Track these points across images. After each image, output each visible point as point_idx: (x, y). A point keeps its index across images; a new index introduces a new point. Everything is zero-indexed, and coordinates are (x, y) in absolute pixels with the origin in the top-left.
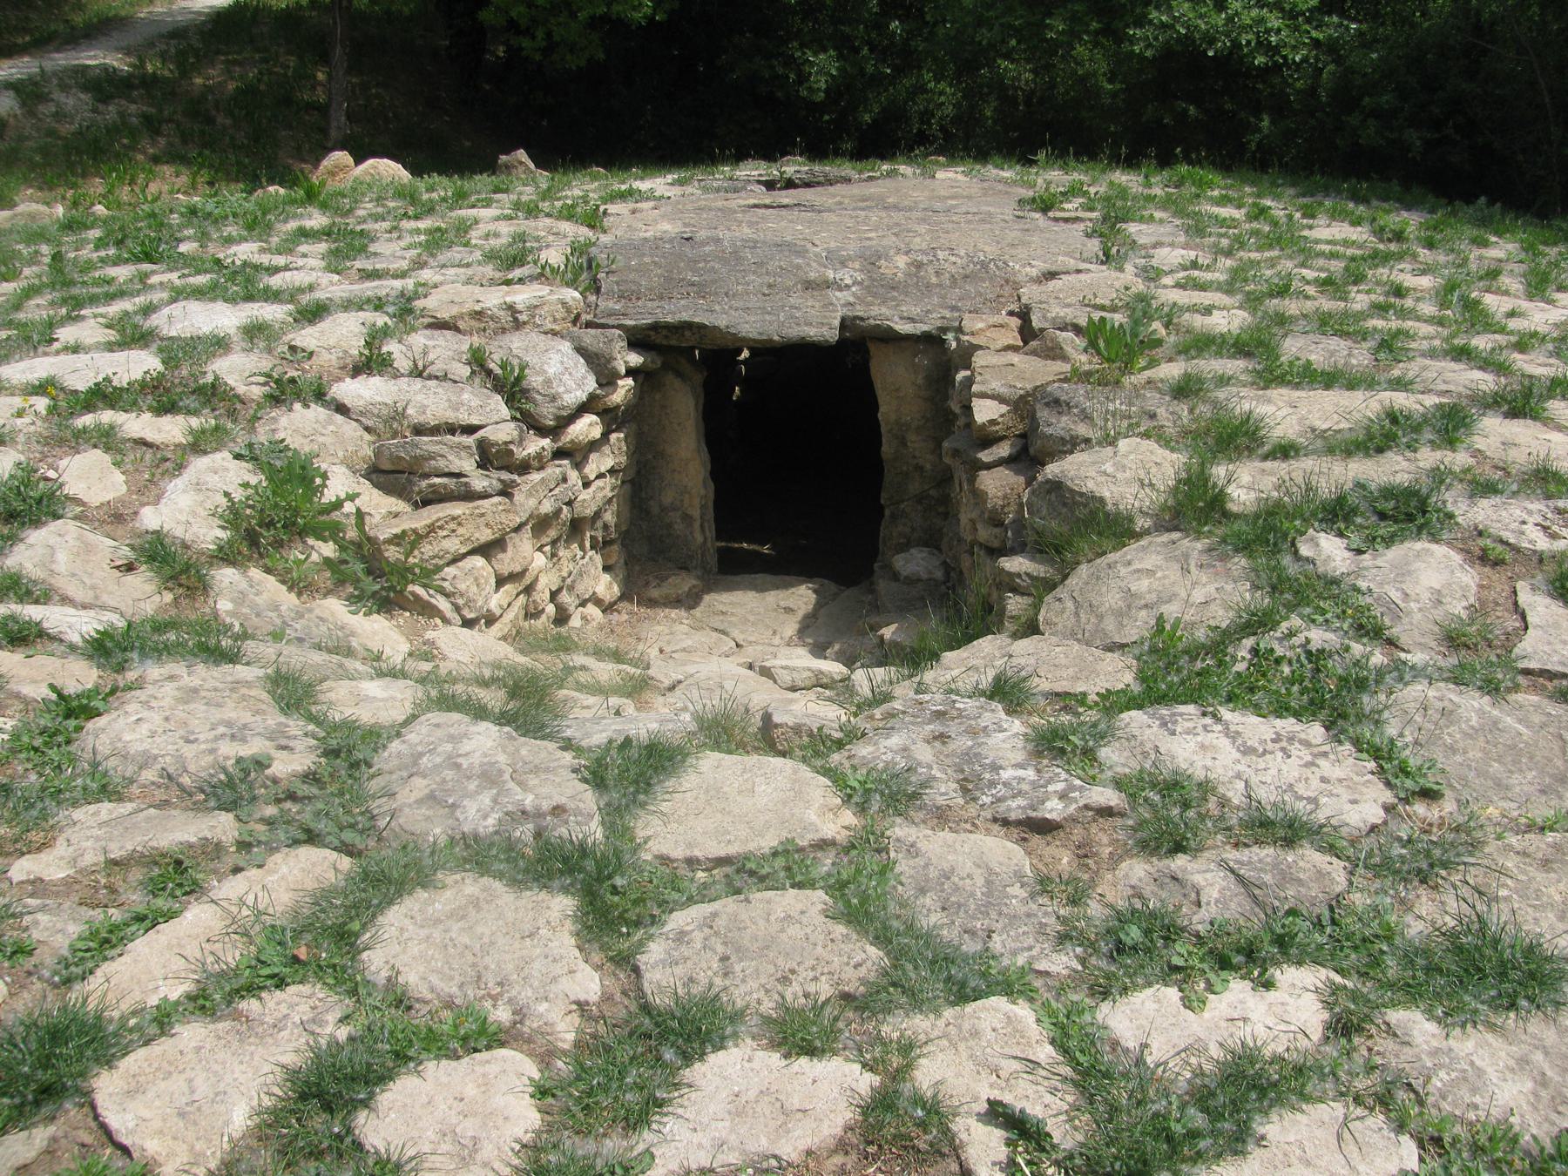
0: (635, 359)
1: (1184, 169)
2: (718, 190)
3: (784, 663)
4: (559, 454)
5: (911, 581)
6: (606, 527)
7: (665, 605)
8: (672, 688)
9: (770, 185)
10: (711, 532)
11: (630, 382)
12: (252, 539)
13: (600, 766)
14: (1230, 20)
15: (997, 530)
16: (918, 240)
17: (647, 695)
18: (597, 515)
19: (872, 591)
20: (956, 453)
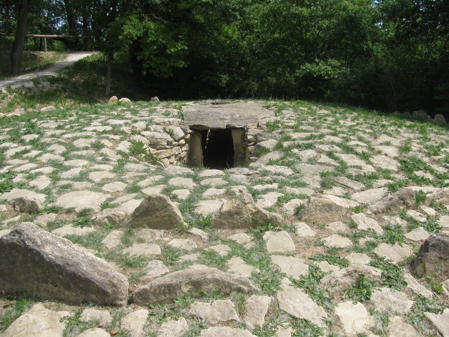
1: (299, 101)
4: (178, 145)
9: (213, 104)
12: (133, 152)
14: (319, 68)
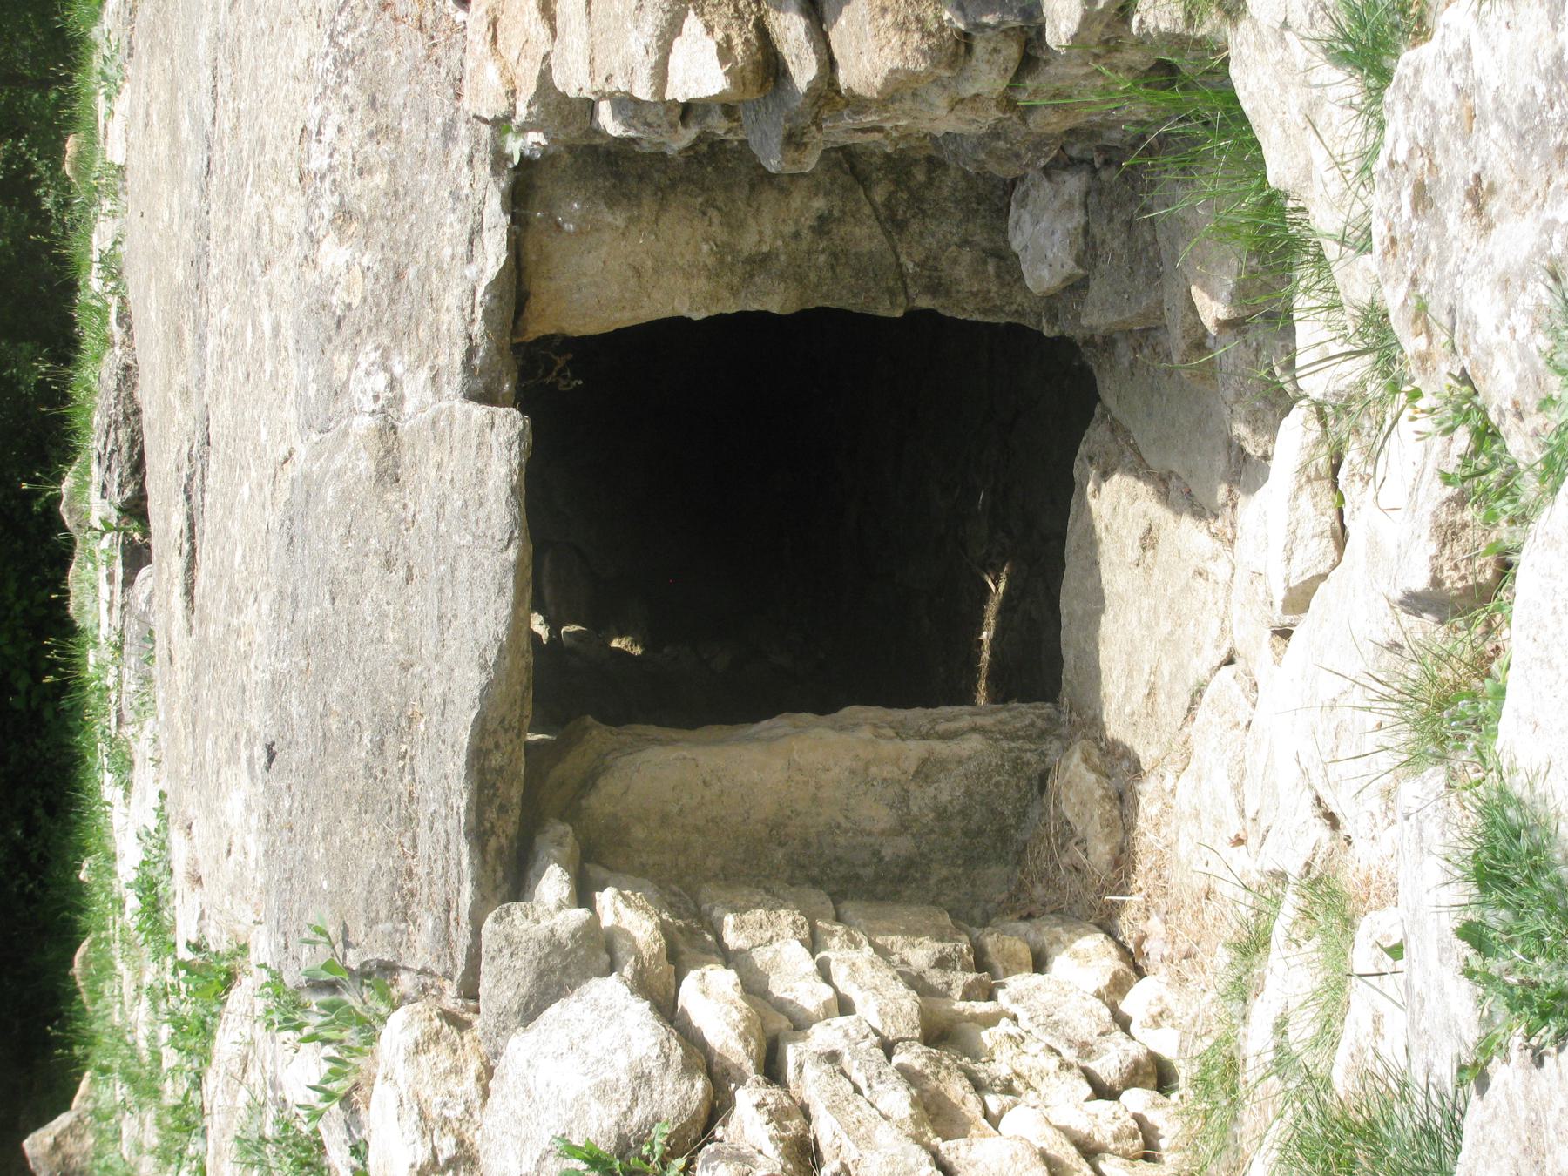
0: (553, 883)
2: (146, 680)
3: (1277, 554)
4: (772, 1068)
5: (1088, 251)
6: (942, 963)
7: (1129, 829)
8: (1332, 820)
9: (136, 556)
10: (960, 717)
11: (606, 899)
13: (1528, 999)
15: (980, 47)
16: (280, 215)
17: (1349, 879)
18: (915, 982)
19: (1109, 342)
20: (794, 140)
